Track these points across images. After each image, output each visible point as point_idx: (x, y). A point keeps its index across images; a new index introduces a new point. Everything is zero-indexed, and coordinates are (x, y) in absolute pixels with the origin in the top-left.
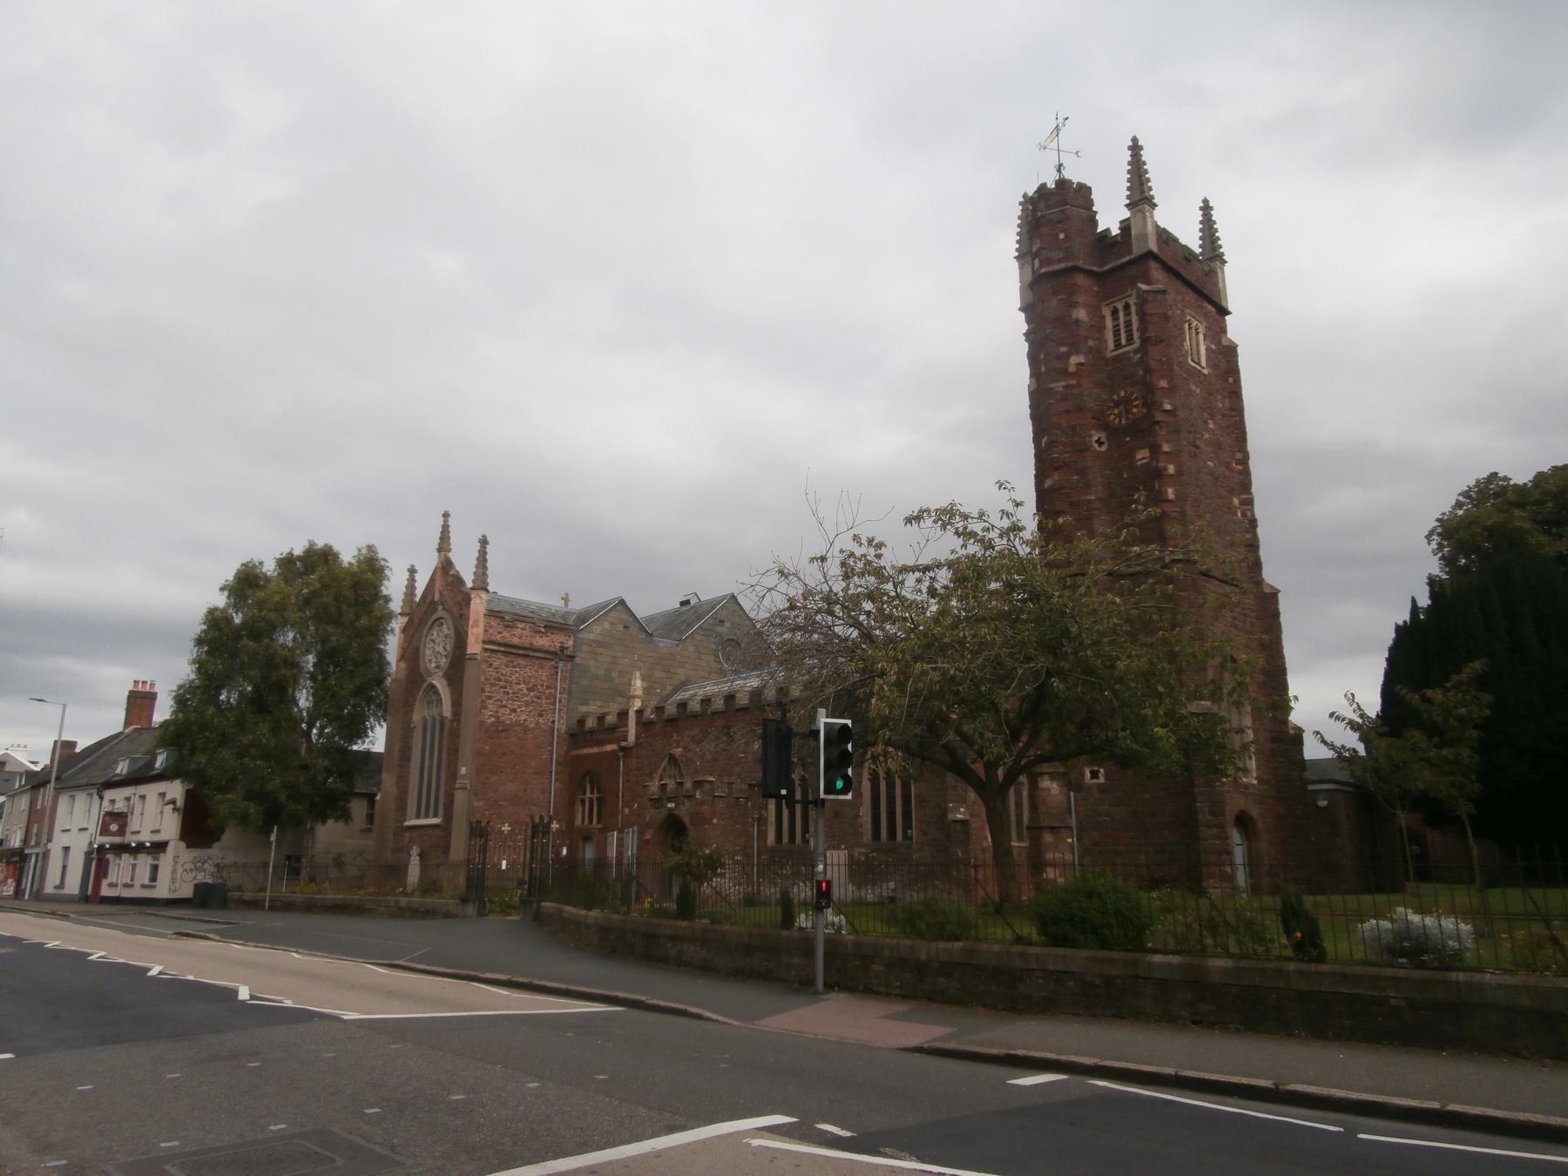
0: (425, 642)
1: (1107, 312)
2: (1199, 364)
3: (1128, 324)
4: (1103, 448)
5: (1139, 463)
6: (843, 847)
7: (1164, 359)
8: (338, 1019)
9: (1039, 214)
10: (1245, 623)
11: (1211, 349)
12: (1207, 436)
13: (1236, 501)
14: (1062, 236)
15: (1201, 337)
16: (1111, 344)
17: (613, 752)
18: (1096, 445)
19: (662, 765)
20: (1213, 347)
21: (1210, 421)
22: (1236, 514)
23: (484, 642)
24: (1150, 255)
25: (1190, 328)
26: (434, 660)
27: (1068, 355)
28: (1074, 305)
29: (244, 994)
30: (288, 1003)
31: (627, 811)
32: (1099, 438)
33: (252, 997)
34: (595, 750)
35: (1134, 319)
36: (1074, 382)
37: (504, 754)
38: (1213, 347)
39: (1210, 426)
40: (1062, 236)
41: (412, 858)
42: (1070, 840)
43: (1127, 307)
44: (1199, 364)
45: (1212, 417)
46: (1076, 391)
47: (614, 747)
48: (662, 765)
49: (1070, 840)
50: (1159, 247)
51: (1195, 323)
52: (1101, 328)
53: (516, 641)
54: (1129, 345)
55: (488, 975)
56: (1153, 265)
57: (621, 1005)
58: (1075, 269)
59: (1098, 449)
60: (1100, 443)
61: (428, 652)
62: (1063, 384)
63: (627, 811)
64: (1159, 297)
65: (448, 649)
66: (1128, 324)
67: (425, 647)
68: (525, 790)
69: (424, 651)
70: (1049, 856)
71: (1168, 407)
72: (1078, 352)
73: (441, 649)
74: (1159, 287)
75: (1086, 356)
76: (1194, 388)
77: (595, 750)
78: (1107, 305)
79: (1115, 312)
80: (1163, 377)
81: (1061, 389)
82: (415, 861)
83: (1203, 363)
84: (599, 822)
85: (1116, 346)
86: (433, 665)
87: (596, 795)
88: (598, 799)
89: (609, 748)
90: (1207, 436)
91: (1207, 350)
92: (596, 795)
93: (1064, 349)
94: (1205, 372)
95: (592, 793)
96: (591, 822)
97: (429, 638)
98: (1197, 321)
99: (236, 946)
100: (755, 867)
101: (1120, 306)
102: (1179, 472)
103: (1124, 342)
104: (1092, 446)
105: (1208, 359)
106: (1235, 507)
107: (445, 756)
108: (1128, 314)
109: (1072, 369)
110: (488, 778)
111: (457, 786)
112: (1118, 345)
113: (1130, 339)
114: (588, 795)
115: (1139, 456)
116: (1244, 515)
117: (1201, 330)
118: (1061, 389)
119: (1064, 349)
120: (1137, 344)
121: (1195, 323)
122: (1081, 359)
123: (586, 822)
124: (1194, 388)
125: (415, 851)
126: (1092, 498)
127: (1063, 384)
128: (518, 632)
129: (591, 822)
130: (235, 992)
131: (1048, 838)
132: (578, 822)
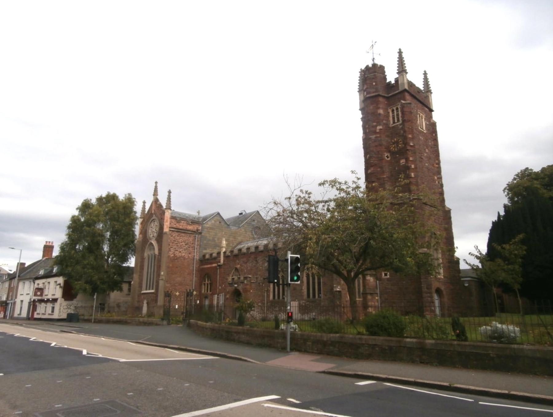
1: (390, 111)
2: (423, 129)
3: (398, 115)
4: (389, 159)
5: (401, 164)
8: (118, 361)
10: (439, 221)
13: (436, 178)
14: (374, 84)
15: (423, 119)
16: (392, 122)
17: (215, 267)
18: (386, 158)
22: (436, 182)
24: (405, 90)
27: (376, 126)
28: (379, 108)
29: (85, 352)
30: (100, 356)
31: (220, 287)
33: (88, 354)
34: (209, 266)
36: (378, 135)
40: (374, 84)
43: (397, 109)
44: (423, 129)
46: (379, 139)
50: (409, 87)
51: (421, 115)
53: (181, 227)
58: (379, 95)
60: (388, 157)
61: (150, 231)
62: (374, 136)
63: (220, 287)
64: (409, 105)
66: (398, 115)
67: (149, 230)
70: (370, 304)
71: (412, 144)
72: (380, 125)
74: (408, 102)
77: (209, 266)
78: (390, 108)
79: (393, 111)
80: (410, 134)
83: (424, 128)
84: (210, 291)
87: (209, 282)
90: (425, 155)
91: (425, 124)
94: (425, 132)
96: (207, 291)
100: (266, 308)
101: (395, 108)
102: (416, 168)
103: (396, 121)
104: (385, 158)
105: (426, 127)
108: (397, 111)
109: (378, 131)
112: (394, 122)
113: (398, 120)
114: (207, 282)
117: (424, 117)
118: (374, 138)
120: (401, 122)
121: (421, 115)
122: (381, 127)
123: (206, 291)
125: (145, 302)
127: (374, 136)
129: (207, 291)
130: (82, 352)
132: (203, 291)
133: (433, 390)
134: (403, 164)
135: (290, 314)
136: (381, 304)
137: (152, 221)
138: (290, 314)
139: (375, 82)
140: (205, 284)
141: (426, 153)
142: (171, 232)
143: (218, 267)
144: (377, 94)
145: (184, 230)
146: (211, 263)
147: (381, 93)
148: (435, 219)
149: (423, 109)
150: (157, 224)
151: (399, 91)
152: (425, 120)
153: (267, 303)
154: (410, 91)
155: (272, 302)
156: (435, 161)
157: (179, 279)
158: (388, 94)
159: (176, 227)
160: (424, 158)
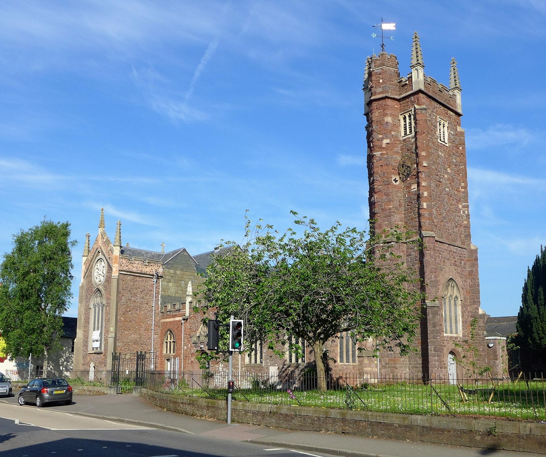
0: (94, 269)
1: (401, 118)
2: (444, 142)
3: (410, 123)
4: (398, 183)
5: (412, 190)
6: (276, 365)
7: (424, 142)
8: (50, 430)
9: (372, 70)
10: (461, 263)
11: (451, 134)
12: (446, 176)
13: (460, 206)
14: (381, 81)
15: (446, 128)
16: (403, 134)
17: (180, 321)
18: (394, 182)
19: (201, 327)
20: (452, 133)
21: (448, 169)
22: (460, 212)
23: (120, 270)
24: (420, 91)
25: (440, 125)
26: (98, 278)
27: (382, 139)
28: (386, 115)
29: (17, 422)
30: (33, 425)
31: (185, 347)
32: (396, 179)
33: (20, 423)
34: (172, 320)
35: (413, 122)
36: (385, 152)
37: (131, 321)
38: (452, 133)
39: (448, 171)
40: (381, 81)
41: (91, 368)
42: (376, 362)
43: (410, 116)
44: (444, 142)
45: (449, 166)
46: (385, 156)
47: (181, 318)
48: (201, 327)
49: (376, 362)
50: (425, 87)
51: (442, 122)
52: (398, 126)
53: (134, 270)
54: (411, 134)
55: (111, 417)
56: (421, 95)
57: (156, 428)
58: (387, 97)
59: (395, 184)
60: (396, 181)
61: (96, 274)
62: (380, 153)
63: (185, 347)
64: (423, 111)
65: (104, 273)
66: (410, 123)
67: (94, 272)
68: (140, 338)
69: (94, 273)
70: (365, 369)
71: (425, 165)
72: (387, 138)
73: (101, 273)
74: (424, 107)
75: (391, 140)
76: (440, 154)
77: (172, 320)
78: (401, 115)
79: (405, 118)
80: (423, 150)
81: (379, 155)
82: (92, 369)
83: (446, 141)
84: (174, 352)
85: (405, 134)
86: (98, 280)
87: (172, 340)
88: (174, 342)
89: (178, 319)
90: (446, 176)
91: (449, 135)
92: (172, 340)
93: (380, 136)
94: (447, 145)
95: (171, 339)
96: (170, 352)
97: (96, 267)
98: (444, 120)
99: (15, 406)
100: (240, 375)
101: (407, 115)
102: (430, 195)
103: (408, 133)
104: (392, 182)
105: (449, 138)
106: (459, 209)
107: (104, 322)
108: (410, 119)
109: (384, 146)
110: (124, 332)
111: (109, 336)
112: (406, 134)
113: (411, 132)
114: (169, 340)
115: (412, 188)
116: (464, 212)
117: (446, 125)
118: (379, 155)
119: (380, 136)
120: (413, 134)
121: (442, 122)
122: (388, 141)
123: (168, 352)
124: (440, 154)
125: (92, 365)
126: (391, 207)
127: (380, 153)
128: (135, 265)
129: (170, 352)
130: (14, 421)
131: (366, 361)
132: (165, 352)
133: (308, 452)
134: (414, 190)
135: (231, 383)
136: (380, 369)
137: (98, 261)
138: (231, 383)
139: (382, 79)
140: (167, 342)
141: (447, 173)
142: (122, 276)
143: (183, 322)
144: (384, 95)
145: (138, 273)
146: (174, 316)
147: (389, 95)
148: (455, 262)
149: (447, 114)
150: (104, 265)
151: (412, 92)
152: (448, 129)
153: (242, 368)
154: (427, 92)
155: (247, 366)
156: (460, 185)
157: (134, 336)
158: (400, 94)
159: (128, 270)
160: (443, 181)
